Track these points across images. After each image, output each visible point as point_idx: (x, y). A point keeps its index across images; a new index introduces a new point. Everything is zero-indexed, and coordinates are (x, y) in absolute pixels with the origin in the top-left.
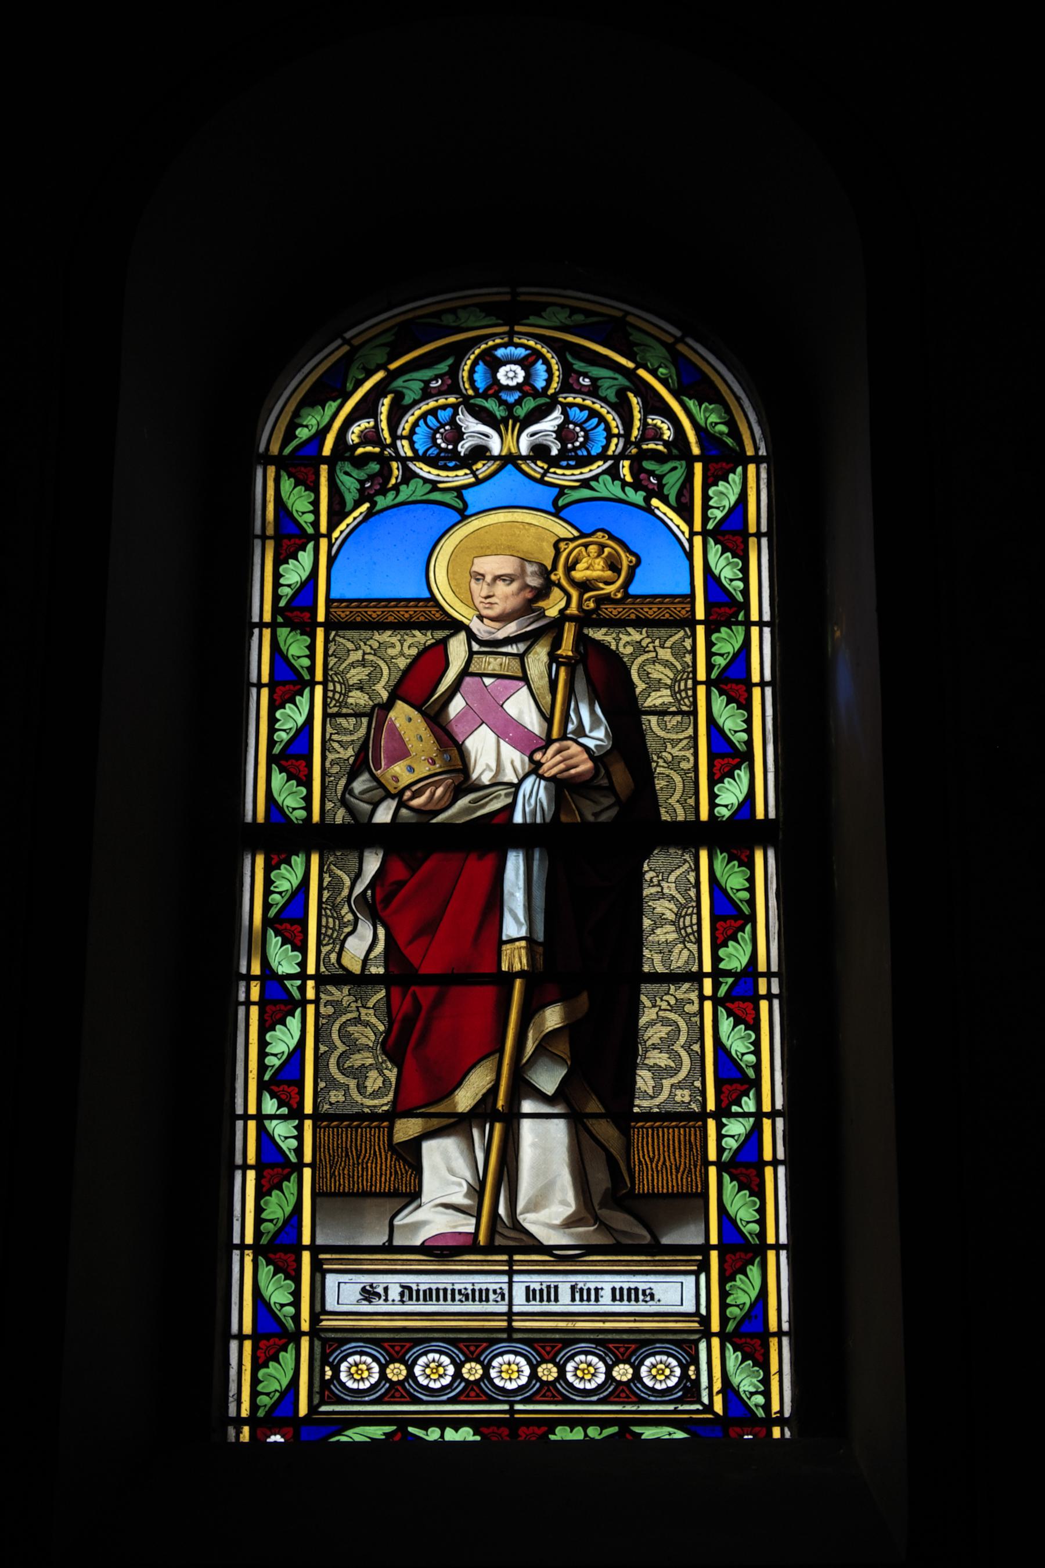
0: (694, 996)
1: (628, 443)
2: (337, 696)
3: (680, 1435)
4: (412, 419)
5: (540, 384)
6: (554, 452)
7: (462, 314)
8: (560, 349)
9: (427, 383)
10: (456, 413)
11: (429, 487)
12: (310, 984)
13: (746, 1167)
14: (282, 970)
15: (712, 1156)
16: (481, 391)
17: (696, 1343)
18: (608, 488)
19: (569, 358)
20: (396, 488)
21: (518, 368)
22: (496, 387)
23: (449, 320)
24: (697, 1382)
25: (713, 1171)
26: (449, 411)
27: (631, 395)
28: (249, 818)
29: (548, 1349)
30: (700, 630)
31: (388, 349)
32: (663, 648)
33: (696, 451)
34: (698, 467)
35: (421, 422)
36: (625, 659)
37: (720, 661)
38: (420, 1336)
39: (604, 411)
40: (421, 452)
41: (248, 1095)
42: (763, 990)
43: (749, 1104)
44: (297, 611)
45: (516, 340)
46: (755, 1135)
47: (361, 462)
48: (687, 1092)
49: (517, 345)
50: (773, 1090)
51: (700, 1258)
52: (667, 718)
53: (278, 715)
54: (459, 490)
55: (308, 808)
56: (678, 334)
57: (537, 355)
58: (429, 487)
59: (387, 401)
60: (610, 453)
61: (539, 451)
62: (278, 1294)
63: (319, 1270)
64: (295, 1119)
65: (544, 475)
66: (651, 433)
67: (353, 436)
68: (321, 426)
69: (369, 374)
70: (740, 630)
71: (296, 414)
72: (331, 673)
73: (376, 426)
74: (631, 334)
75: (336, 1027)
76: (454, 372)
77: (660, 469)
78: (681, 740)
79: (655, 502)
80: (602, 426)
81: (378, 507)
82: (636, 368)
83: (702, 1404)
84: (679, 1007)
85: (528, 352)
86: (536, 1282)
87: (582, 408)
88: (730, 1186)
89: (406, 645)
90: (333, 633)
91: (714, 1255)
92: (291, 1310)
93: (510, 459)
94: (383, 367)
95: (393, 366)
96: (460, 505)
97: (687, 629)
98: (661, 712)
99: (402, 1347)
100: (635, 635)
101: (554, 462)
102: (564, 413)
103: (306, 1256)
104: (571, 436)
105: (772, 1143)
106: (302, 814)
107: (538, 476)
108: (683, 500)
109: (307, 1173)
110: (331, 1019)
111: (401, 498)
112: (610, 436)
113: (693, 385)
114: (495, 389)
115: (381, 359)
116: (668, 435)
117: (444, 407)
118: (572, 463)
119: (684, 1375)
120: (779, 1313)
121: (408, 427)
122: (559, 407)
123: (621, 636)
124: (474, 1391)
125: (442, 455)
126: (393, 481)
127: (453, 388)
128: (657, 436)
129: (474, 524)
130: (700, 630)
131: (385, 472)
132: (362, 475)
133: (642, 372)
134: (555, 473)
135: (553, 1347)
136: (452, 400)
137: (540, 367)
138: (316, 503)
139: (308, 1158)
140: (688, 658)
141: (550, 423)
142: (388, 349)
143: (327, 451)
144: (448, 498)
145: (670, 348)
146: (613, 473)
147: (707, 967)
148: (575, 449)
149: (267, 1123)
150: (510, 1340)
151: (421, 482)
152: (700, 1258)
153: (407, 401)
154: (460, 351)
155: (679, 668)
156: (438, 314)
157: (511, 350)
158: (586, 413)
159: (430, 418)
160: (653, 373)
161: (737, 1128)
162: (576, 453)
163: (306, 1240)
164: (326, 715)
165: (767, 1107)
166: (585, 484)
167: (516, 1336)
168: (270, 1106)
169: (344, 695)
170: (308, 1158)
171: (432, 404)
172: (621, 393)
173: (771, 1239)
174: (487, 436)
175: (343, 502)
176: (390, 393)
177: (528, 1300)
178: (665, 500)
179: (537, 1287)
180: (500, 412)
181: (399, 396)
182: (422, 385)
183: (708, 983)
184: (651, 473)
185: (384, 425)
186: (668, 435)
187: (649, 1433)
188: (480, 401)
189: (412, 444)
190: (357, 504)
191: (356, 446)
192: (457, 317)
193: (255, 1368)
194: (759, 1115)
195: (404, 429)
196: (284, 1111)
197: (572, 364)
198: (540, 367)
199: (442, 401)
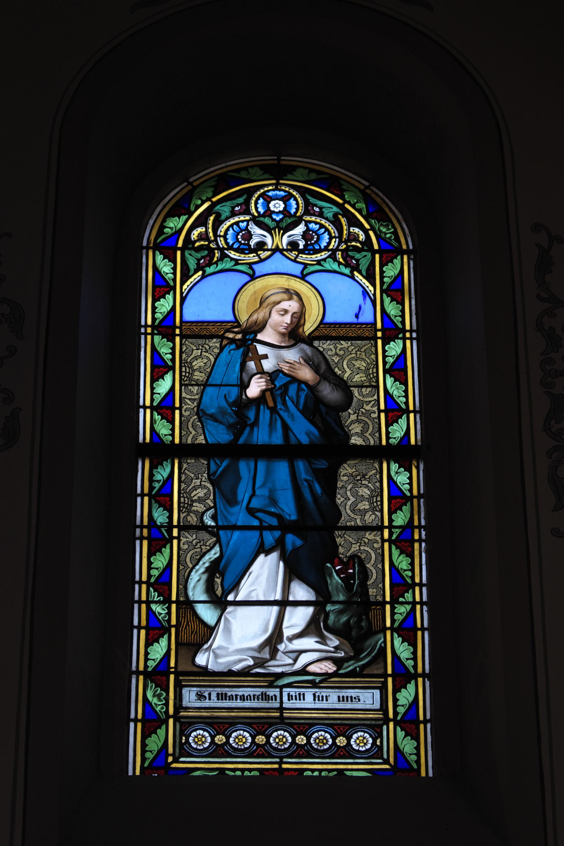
0: (378, 538)
1: (340, 242)
2: (187, 375)
5: (293, 211)
6: (301, 247)
7: (250, 170)
8: (303, 192)
9: (233, 208)
10: (248, 225)
13: (407, 630)
15: (388, 624)
16: (262, 213)
17: (381, 727)
18: (331, 265)
19: (309, 197)
20: (216, 263)
21: (281, 203)
22: (269, 212)
23: (244, 175)
24: (381, 748)
26: (245, 224)
27: (340, 217)
30: (380, 342)
33: (376, 247)
34: (377, 256)
35: (231, 229)
37: (390, 360)
38: (195, 720)
39: (327, 225)
42: (416, 537)
43: (408, 596)
44: (166, 327)
46: (412, 614)
49: (280, 190)
51: (383, 680)
52: (364, 390)
54: (250, 265)
55: (173, 435)
57: (290, 196)
58: (233, 263)
59: (212, 218)
60: (331, 247)
61: (293, 245)
63: (179, 686)
66: (353, 237)
67: (195, 235)
68: (178, 228)
69: (203, 203)
70: (400, 342)
74: (342, 185)
75: (189, 555)
76: (247, 203)
77: (358, 256)
79: (356, 273)
80: (327, 233)
87: (316, 223)
91: (390, 680)
93: (277, 250)
94: (209, 199)
95: (214, 199)
96: (251, 272)
98: (360, 386)
99: (344, 728)
101: (302, 252)
102: (306, 225)
105: (422, 617)
106: (170, 438)
107: (293, 258)
109: (173, 630)
110: (187, 551)
112: (331, 238)
113: (375, 212)
114: (269, 213)
115: (210, 195)
116: (362, 237)
117: (243, 221)
118: (311, 252)
119: (374, 743)
122: (303, 222)
126: (215, 259)
127: (247, 211)
128: (356, 239)
129: (258, 284)
130: (380, 342)
131: (212, 255)
132: (199, 255)
133: (347, 206)
136: (248, 218)
137: (293, 202)
138: (174, 269)
140: (373, 357)
141: (300, 229)
145: (363, 192)
146: (333, 256)
147: (386, 523)
152: (383, 680)
153: (223, 217)
154: (250, 192)
156: (238, 171)
157: (278, 193)
159: (235, 226)
160: (353, 206)
161: (402, 610)
166: (319, 262)
168: (155, 596)
169: (191, 374)
170: (174, 622)
171: (236, 219)
172: (335, 215)
174: (265, 237)
175: (188, 269)
176: (214, 213)
178: (360, 272)
180: (272, 224)
181: (218, 215)
184: (353, 258)
185: (210, 230)
186: (362, 237)
188: (262, 219)
189: (226, 240)
190: (196, 271)
191: (195, 242)
192: (249, 173)
194: (414, 603)
198: (293, 202)
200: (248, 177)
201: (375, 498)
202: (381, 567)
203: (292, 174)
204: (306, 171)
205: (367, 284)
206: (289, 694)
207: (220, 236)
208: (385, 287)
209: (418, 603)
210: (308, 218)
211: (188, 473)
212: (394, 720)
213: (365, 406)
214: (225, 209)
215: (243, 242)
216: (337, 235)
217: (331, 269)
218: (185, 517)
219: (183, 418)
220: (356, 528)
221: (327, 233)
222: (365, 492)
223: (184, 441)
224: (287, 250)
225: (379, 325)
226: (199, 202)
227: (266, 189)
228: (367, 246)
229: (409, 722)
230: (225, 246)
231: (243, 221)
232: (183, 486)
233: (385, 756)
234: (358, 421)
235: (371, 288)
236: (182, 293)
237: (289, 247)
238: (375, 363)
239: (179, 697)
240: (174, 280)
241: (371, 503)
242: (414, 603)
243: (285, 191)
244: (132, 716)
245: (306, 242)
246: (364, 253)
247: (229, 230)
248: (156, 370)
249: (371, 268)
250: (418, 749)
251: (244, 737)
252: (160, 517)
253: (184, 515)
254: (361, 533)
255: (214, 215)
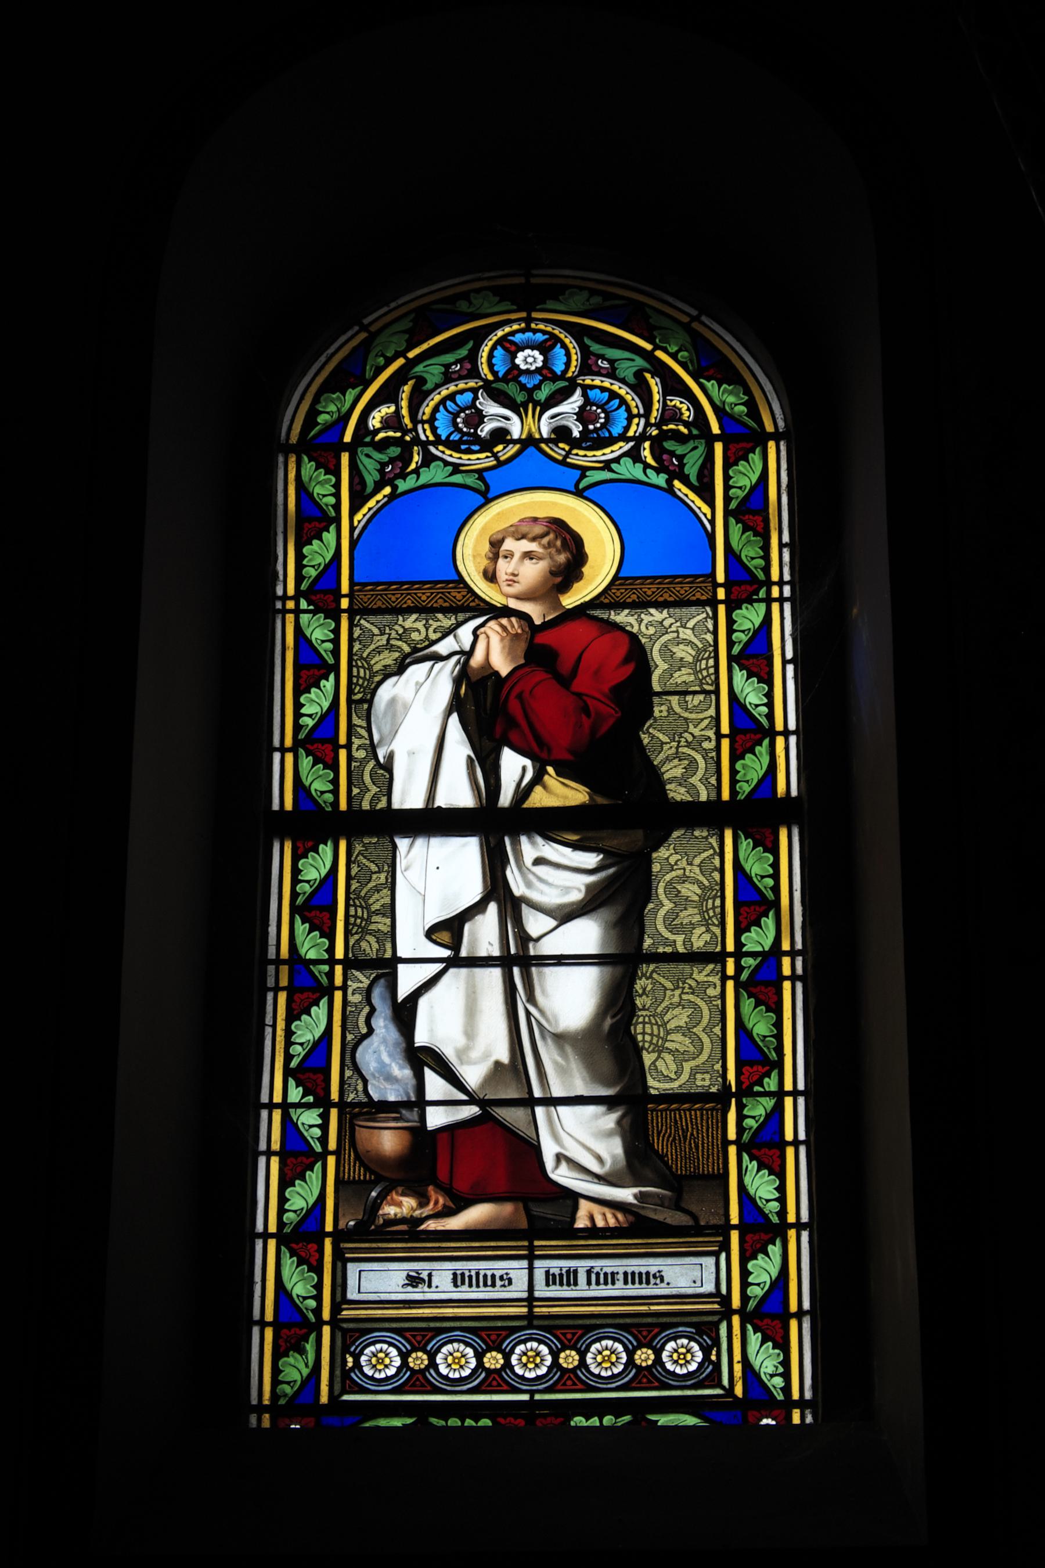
1: (648, 424)
3: (690, 1420)
4: (432, 404)
5: (559, 368)
6: (576, 434)
8: (578, 333)
10: (476, 398)
11: (450, 469)
12: (339, 969)
14: (312, 955)
15: (732, 1135)
16: (500, 375)
17: (716, 1326)
18: (628, 469)
21: (536, 353)
22: (516, 372)
23: (463, 306)
24: (717, 1365)
25: (732, 1150)
26: (469, 396)
27: (648, 376)
28: (276, 806)
29: (569, 1336)
30: (722, 609)
31: (407, 336)
32: (685, 628)
33: (716, 429)
34: (719, 448)
35: (441, 408)
36: (643, 641)
39: (622, 392)
40: (443, 438)
41: (276, 1085)
42: (787, 971)
43: (771, 1084)
45: (533, 326)
47: (382, 446)
48: (707, 1076)
49: (535, 331)
50: (794, 1071)
51: (721, 1239)
52: (689, 698)
53: (302, 700)
54: (480, 472)
55: (335, 792)
56: (694, 313)
57: (555, 340)
58: (450, 469)
59: (407, 388)
60: (631, 433)
61: (561, 433)
62: (299, 1286)
63: (340, 1259)
64: (319, 1107)
65: (566, 456)
66: (670, 415)
67: (375, 421)
69: (389, 362)
71: (316, 400)
72: (355, 658)
73: (398, 411)
77: (680, 450)
78: (702, 720)
79: (677, 484)
80: (624, 407)
81: (399, 491)
82: (654, 350)
83: (723, 1388)
84: (700, 990)
85: (546, 337)
86: (556, 1266)
87: (603, 389)
88: (748, 1004)
89: (431, 630)
90: (358, 617)
91: (735, 1236)
92: (312, 1303)
93: (529, 442)
95: (411, 355)
97: (708, 609)
100: (656, 615)
101: (575, 444)
102: (585, 395)
103: (328, 1243)
104: (593, 416)
105: (794, 1122)
107: (560, 458)
108: (705, 480)
109: (331, 1160)
111: (422, 480)
112: (630, 417)
113: (711, 365)
116: (687, 414)
117: (462, 392)
120: (800, 1294)
121: (428, 411)
123: (643, 616)
124: (495, 1380)
125: (465, 438)
126: (413, 466)
127: (474, 373)
130: (722, 609)
133: (659, 354)
134: (577, 455)
135: (574, 1334)
136: (472, 384)
139: (332, 1145)
141: (573, 404)
142: (407, 336)
143: (348, 438)
144: (471, 480)
146: (634, 455)
147: (730, 947)
148: (596, 430)
149: (292, 1111)
150: (530, 1326)
151: (441, 464)
152: (721, 1239)
153: (429, 386)
154: (479, 336)
155: (700, 646)
158: (606, 394)
159: (449, 403)
162: (598, 435)
163: (329, 1227)
164: (350, 701)
165: (788, 1086)
166: (607, 465)
167: (536, 1323)
168: (295, 1094)
170: (332, 1145)
171: (452, 388)
172: (639, 374)
173: (791, 1218)
175: (363, 482)
177: (547, 1285)
178: (686, 481)
179: (557, 1271)
180: (520, 398)
181: (421, 381)
182: (443, 369)
183: (730, 964)
184: (672, 454)
185: (405, 412)
186: (687, 414)
187: (664, 1420)
189: (434, 430)
190: (378, 487)
191: (377, 431)
192: (470, 303)
193: (277, 1356)
195: (424, 413)
196: (310, 1099)
197: (589, 347)
199: (462, 385)
200: (470, 310)
201: (710, 902)
202: (719, 1033)
203: (556, 299)
204: (585, 294)
205: (699, 502)
206: (547, 1273)
207: (423, 422)
208: (733, 505)
209: (789, 1094)
210: (588, 382)
211: (364, 861)
212: (742, 1312)
213: (691, 728)
214: (432, 371)
215: (465, 430)
216: (642, 411)
217: (630, 477)
218: (358, 941)
219: (354, 764)
220: (674, 957)
221: (624, 407)
222: (690, 891)
223: (355, 804)
224: (547, 441)
225: (721, 577)
226: (381, 361)
227: (507, 329)
228: (696, 428)
229: (769, 1315)
230: (431, 438)
231: (462, 392)
232: (355, 885)
233: (725, 1382)
234: (678, 756)
235: (706, 509)
236: (352, 529)
237: (553, 436)
238: (711, 649)
239: (340, 1284)
240: (337, 507)
241: (701, 913)
242: (780, 1094)
243: (544, 332)
244: (787, 606)
245: (585, 427)
246: (691, 444)
247: (438, 411)
248: (304, 673)
249: (706, 472)
250: (787, 1366)
251: (449, 1365)
252: (311, 947)
253: (357, 937)
254: (686, 968)
255: (411, 383)
